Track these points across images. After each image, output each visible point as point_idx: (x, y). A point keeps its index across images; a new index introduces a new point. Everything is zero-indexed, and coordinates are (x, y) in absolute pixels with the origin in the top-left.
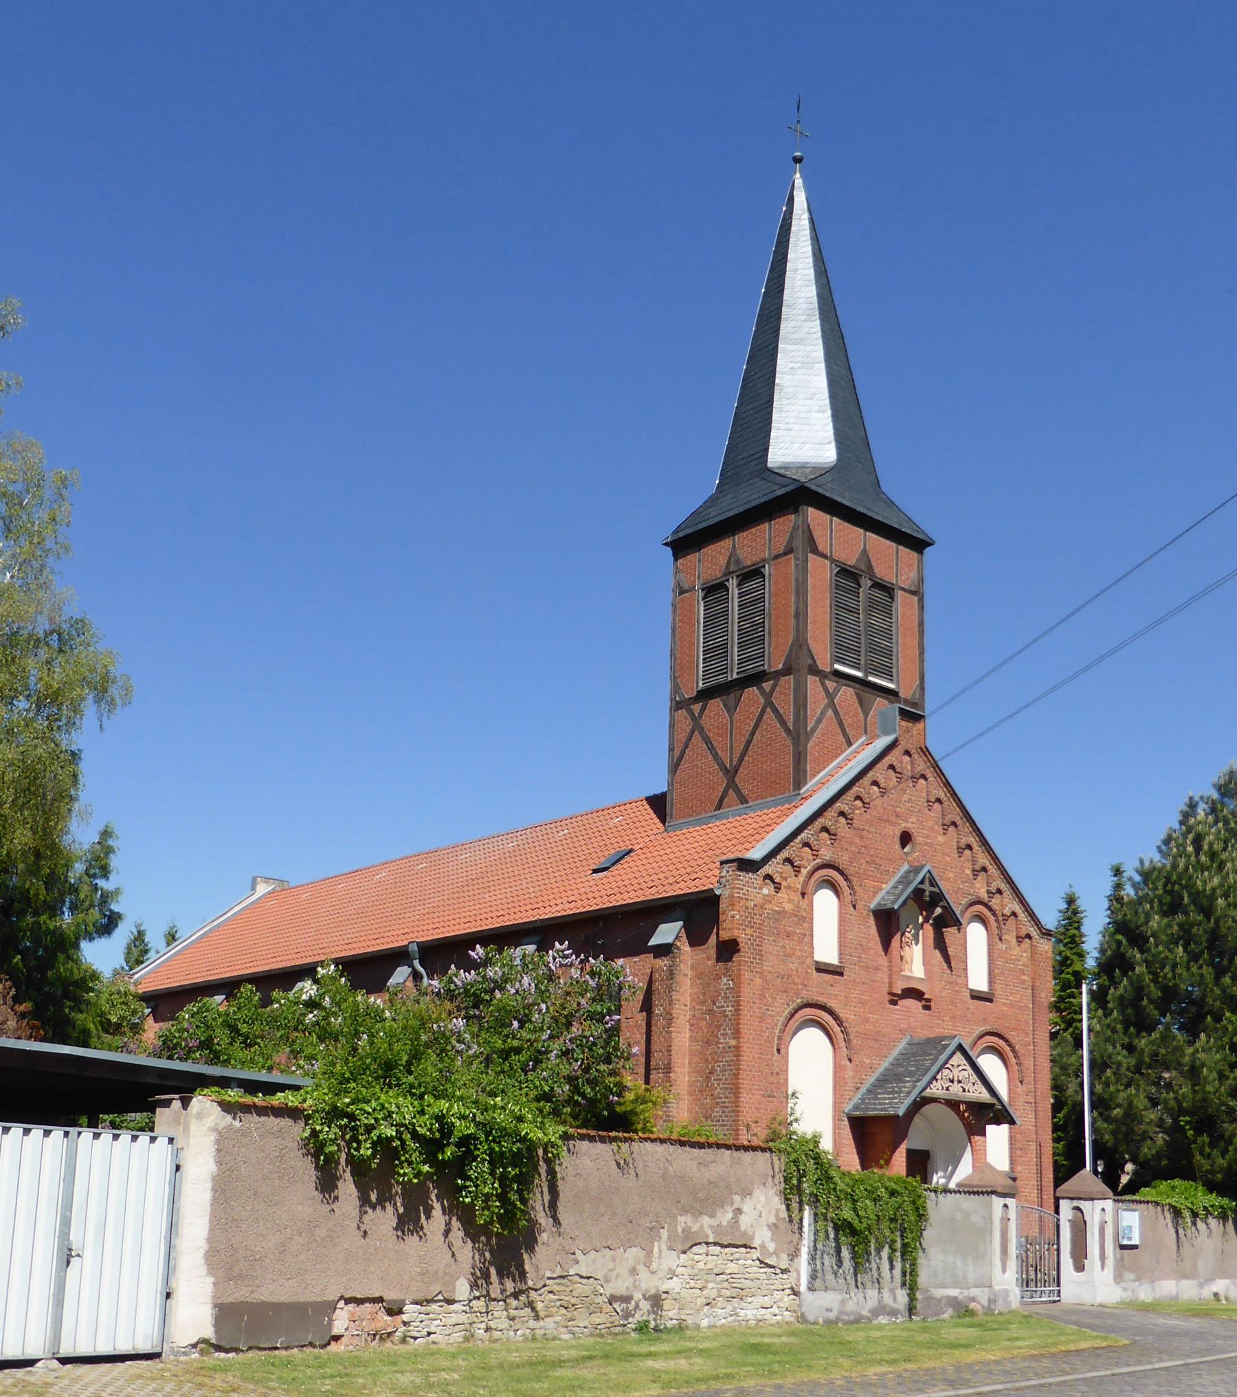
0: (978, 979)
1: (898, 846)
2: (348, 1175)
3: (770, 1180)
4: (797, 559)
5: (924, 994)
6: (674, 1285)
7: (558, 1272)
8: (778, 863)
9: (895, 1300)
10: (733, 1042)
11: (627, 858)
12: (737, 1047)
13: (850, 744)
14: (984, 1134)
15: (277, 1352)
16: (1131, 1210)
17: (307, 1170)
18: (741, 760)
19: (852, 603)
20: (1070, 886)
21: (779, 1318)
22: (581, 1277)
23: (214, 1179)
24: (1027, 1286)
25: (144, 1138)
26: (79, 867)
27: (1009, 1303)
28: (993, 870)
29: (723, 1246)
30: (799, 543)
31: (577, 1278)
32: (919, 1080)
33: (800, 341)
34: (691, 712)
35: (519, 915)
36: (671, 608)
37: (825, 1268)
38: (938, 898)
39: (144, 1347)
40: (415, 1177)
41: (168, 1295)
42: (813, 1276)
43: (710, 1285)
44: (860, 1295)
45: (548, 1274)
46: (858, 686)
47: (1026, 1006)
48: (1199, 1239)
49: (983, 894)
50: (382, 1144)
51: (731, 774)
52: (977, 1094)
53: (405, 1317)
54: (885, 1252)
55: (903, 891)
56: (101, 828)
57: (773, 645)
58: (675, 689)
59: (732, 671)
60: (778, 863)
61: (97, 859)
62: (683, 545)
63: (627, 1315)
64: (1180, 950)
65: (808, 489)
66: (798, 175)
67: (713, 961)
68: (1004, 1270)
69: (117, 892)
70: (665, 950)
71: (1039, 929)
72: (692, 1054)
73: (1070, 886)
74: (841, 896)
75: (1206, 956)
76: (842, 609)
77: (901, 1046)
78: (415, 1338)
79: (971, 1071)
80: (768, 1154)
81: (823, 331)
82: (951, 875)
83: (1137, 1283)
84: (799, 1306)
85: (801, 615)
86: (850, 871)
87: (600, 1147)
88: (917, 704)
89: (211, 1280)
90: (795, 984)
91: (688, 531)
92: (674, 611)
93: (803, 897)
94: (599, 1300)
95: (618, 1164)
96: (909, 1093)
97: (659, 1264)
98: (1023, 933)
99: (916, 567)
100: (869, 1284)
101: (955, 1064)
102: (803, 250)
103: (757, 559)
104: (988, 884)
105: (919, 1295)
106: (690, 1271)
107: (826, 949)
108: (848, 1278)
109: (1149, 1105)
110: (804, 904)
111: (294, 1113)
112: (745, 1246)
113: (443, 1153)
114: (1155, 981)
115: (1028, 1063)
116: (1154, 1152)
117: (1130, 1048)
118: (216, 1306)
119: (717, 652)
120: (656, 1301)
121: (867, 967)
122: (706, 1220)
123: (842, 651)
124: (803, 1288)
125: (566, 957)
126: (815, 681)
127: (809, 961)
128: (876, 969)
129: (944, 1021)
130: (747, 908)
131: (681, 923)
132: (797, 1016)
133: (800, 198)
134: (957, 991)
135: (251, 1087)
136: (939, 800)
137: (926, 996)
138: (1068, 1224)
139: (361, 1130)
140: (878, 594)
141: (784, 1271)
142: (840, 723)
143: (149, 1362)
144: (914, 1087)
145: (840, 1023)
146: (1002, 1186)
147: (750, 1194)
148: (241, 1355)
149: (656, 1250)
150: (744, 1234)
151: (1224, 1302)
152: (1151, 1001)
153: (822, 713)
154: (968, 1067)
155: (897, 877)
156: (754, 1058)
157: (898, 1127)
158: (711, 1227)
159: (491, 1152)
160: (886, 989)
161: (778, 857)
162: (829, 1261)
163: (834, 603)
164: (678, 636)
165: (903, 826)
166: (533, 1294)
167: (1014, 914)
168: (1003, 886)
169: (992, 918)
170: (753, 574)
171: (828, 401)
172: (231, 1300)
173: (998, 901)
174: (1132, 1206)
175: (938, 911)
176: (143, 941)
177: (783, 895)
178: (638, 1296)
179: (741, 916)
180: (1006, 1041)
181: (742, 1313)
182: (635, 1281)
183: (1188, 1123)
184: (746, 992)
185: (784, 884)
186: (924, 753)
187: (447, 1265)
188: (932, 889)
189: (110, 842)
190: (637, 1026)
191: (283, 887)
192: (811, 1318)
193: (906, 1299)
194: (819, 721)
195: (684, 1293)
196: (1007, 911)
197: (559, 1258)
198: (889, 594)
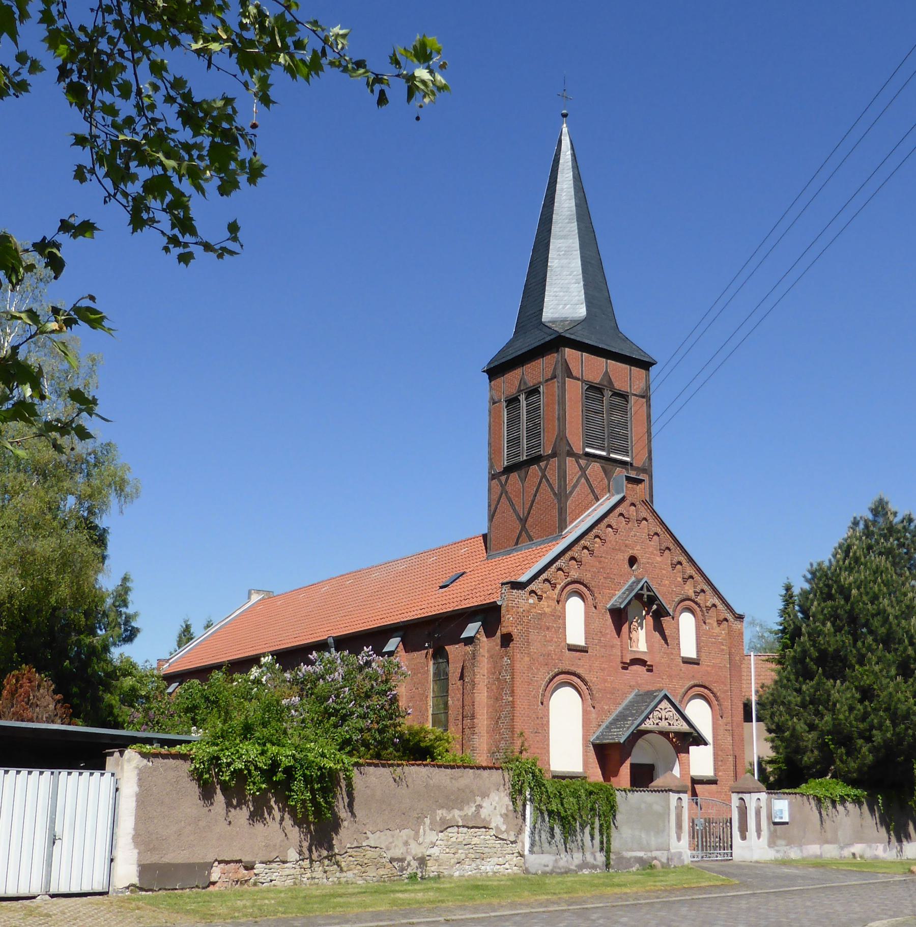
0: (688, 649)
1: (627, 566)
2: (218, 791)
3: (502, 787)
4: (558, 382)
5: (646, 662)
6: (435, 851)
7: (355, 844)
9: (595, 859)
10: (511, 699)
11: (461, 578)
12: (513, 702)
13: (597, 500)
14: (688, 752)
15: (176, 891)
17: (194, 789)
18: (529, 513)
19: (599, 408)
20: (788, 579)
21: (510, 871)
22: (371, 847)
23: (137, 795)
24: (706, 850)
25: (97, 774)
26: (109, 601)
27: (683, 861)
28: (698, 577)
29: (468, 827)
30: (559, 372)
31: (369, 848)
32: (636, 719)
33: (564, 237)
34: (500, 481)
35: (479, 599)
36: (487, 412)
38: (653, 599)
39: (98, 888)
40: (257, 791)
41: (112, 860)
42: (533, 845)
43: (460, 851)
44: (569, 857)
45: (349, 846)
46: (603, 461)
48: (839, 817)
49: (691, 593)
50: (237, 773)
51: (523, 521)
52: (679, 727)
53: (256, 871)
54: (587, 830)
55: (628, 595)
56: (122, 576)
57: (546, 438)
58: (491, 467)
59: (523, 454)
61: (120, 595)
62: (495, 371)
63: (402, 869)
64: (829, 624)
66: (565, 125)
67: (499, 647)
68: (679, 839)
69: (136, 615)
70: (470, 641)
72: (488, 707)
73: (788, 579)
75: (846, 628)
76: (589, 413)
77: (631, 697)
78: (263, 883)
79: (674, 712)
80: (500, 771)
81: (579, 229)
82: (667, 582)
84: (524, 863)
85: (562, 419)
86: (592, 584)
87: (381, 770)
88: (646, 470)
89: (136, 851)
91: (496, 363)
92: (490, 415)
93: (558, 603)
94: (383, 860)
95: (395, 780)
96: (628, 728)
97: (424, 839)
98: (721, 618)
99: (644, 380)
100: (575, 850)
101: (663, 708)
103: (535, 382)
104: (695, 587)
105: (612, 856)
106: (446, 843)
107: (575, 634)
108: (559, 846)
109: (807, 729)
110: (559, 608)
111: (184, 757)
112: (485, 828)
113: (276, 776)
114: (814, 646)
115: (727, 704)
116: (812, 760)
117: (799, 691)
118: (139, 865)
119: (514, 442)
120: (422, 861)
122: (456, 813)
124: (526, 852)
125: (371, 655)
126: (572, 461)
127: (563, 644)
131: (399, 639)
132: (555, 680)
135: (163, 742)
136: (656, 534)
137: (648, 663)
138: (736, 809)
139: (224, 766)
140: (617, 400)
142: (590, 486)
143: (101, 897)
144: (632, 724)
146: (676, 786)
147: (488, 796)
148: (155, 893)
149: (421, 831)
150: (484, 820)
152: (812, 659)
154: (673, 709)
155: (626, 587)
156: (524, 708)
157: (625, 749)
158: (460, 816)
159: (304, 775)
160: (619, 660)
162: (545, 836)
163: (585, 408)
164: (492, 432)
165: (631, 552)
166: (338, 857)
167: (714, 605)
168: (706, 588)
169: (698, 609)
170: (533, 392)
171: (581, 276)
172: (148, 862)
173: (703, 598)
174: (782, 796)
175: (655, 607)
176: (190, 632)
177: (544, 603)
178: (409, 858)
180: (710, 690)
181: (483, 868)
182: (407, 849)
183: (829, 739)
184: (518, 666)
185: (544, 595)
187: (283, 841)
188: (649, 593)
189: (128, 584)
190: (458, 689)
191: (269, 596)
192: (533, 870)
193: (604, 859)
194: (575, 486)
195: (442, 856)
196: (709, 604)
197: (355, 837)
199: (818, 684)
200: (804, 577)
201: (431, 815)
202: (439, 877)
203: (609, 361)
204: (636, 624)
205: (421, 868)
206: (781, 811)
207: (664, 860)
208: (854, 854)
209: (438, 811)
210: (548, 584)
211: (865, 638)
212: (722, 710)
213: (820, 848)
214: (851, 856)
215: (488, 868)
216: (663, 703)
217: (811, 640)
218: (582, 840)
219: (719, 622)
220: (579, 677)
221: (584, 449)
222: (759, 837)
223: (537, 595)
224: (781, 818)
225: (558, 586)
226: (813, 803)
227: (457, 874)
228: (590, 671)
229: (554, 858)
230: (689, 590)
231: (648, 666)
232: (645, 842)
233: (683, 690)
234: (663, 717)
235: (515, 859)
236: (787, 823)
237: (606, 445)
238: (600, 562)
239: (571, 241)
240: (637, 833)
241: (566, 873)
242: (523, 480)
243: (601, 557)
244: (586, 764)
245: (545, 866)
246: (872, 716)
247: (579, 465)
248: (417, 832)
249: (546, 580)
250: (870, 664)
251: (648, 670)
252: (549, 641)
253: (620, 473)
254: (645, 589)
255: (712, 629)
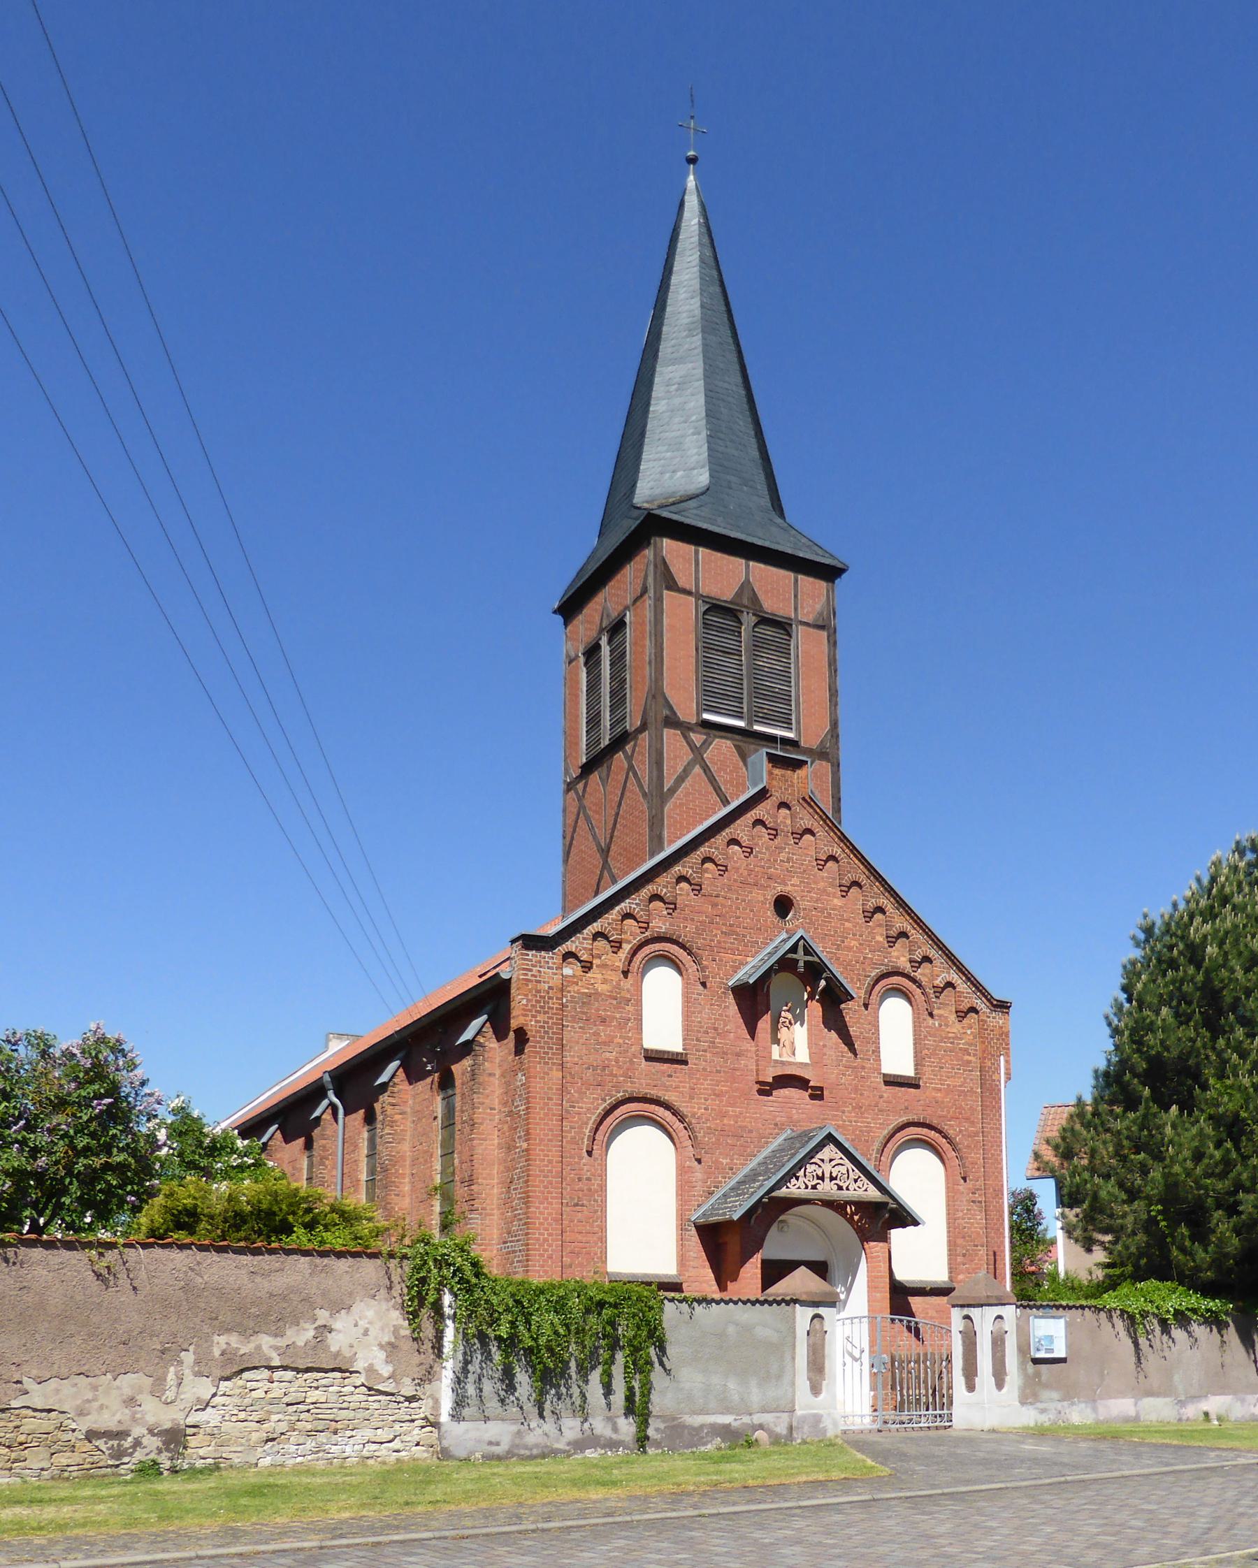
3: (383, 1292)
6: (210, 1417)
8: (584, 939)
9: (615, 1429)
10: (525, 1145)
16: (1054, 1317)
18: (611, 838)
19: (732, 644)
22: (35, 1410)
27: (825, 1431)
28: (916, 935)
29: (298, 1370)
37: (485, 1393)
38: (815, 970)
42: (460, 1403)
47: (971, 1091)
49: (903, 963)
51: (605, 852)
52: (860, 1192)
54: (595, 1376)
60: (584, 939)
62: (570, 608)
63: (119, 1454)
65: (658, 517)
66: (691, 177)
71: (988, 1000)
74: (684, 973)
79: (850, 1166)
80: (378, 1262)
82: (853, 943)
83: (1065, 1403)
90: (616, 1076)
93: (626, 977)
95: (98, 1276)
98: (965, 1006)
101: (826, 1159)
102: (691, 258)
110: (627, 984)
119: (594, 721)
121: (724, 1053)
122: (266, 1342)
123: (710, 696)
124: (444, 1418)
128: (738, 1055)
129: (843, 1112)
130: (539, 991)
132: (618, 1112)
133: (692, 202)
134: (863, 1077)
137: (811, 1084)
140: (769, 632)
141: (410, 1399)
142: (712, 780)
145: (681, 1118)
149: (171, 1376)
150: (337, 1354)
151: (1216, 1422)
152: (1135, 1075)
153: (684, 770)
154: (846, 1161)
158: (276, 1348)
160: (753, 1078)
161: (585, 931)
165: (780, 889)
167: (950, 985)
168: (933, 953)
173: (927, 971)
175: (823, 983)
177: (594, 974)
178: (138, 1431)
179: (528, 1000)
180: (940, 1132)
183: (1159, 1212)
185: (597, 962)
186: (809, 804)
194: (681, 779)
195: (226, 1426)
196: (939, 982)
198: (786, 630)
199: (1145, 1116)
200: (1134, 938)
201: (198, 1346)
202: (217, 1467)
203: (751, 563)
204: (789, 1016)
205: (168, 1450)
206: (1050, 1339)
207: (781, 1429)
208: (1206, 1414)
209: (216, 1338)
210: (605, 942)
211: (1232, 1031)
212: (964, 1166)
213: (1136, 1404)
214: (1202, 1417)
215: (348, 1449)
216: (826, 1149)
217: (1134, 1042)
218: (583, 1395)
219: (962, 1015)
220: (667, 1106)
221: (698, 714)
222: (1000, 1384)
223: (581, 961)
224: (1051, 1351)
225: (624, 945)
226: (1120, 1324)
227: (267, 1461)
228: (692, 1098)
229: (514, 1428)
230: (900, 957)
231: (813, 1088)
232: (736, 1397)
233: (886, 1132)
234: (827, 1175)
235: (417, 1431)
236: (1063, 1360)
237: (745, 710)
238: (714, 905)
239: (690, 365)
240: (716, 1380)
241: (543, 1456)
242: (604, 781)
243: (717, 896)
244: (682, 1261)
245: (490, 1443)
246: (1239, 1167)
247: (691, 744)
248: (160, 1381)
249: (598, 935)
250: (1236, 1075)
251: (812, 1097)
252: (605, 1043)
253: (760, 756)
254: (801, 950)
255: (947, 1025)
